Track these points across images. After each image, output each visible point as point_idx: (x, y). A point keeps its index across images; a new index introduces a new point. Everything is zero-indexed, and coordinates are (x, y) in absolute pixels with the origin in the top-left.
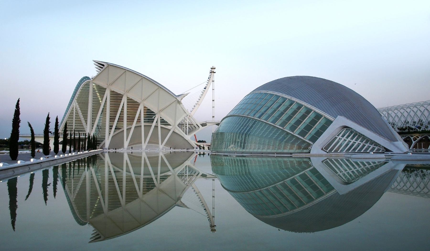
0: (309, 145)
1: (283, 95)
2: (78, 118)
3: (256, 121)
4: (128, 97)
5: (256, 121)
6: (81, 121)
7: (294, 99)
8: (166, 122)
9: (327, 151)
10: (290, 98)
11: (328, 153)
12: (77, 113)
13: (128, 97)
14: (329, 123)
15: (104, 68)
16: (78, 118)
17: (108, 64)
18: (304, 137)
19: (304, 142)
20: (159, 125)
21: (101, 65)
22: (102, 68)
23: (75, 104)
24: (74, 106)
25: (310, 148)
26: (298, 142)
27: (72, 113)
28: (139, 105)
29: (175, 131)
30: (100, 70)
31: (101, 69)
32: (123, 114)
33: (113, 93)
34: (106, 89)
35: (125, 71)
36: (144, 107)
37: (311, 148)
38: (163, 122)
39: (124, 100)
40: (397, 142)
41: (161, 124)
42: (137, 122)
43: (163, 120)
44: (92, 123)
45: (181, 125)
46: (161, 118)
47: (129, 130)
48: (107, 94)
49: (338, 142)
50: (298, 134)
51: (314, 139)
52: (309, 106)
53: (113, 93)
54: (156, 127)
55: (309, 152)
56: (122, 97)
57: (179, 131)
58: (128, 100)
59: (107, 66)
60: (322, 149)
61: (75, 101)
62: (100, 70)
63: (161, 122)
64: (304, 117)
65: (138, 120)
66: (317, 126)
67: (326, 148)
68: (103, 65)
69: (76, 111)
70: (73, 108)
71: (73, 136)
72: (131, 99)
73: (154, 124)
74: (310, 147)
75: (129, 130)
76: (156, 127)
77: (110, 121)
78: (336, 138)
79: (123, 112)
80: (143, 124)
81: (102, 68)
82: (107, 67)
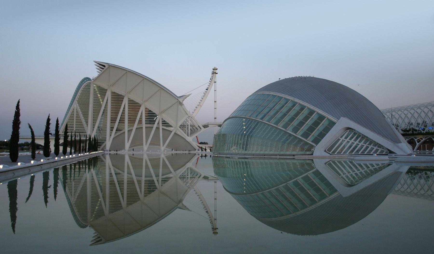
0: (312, 146)
1: (282, 95)
2: (78, 120)
3: (258, 123)
4: (129, 99)
5: (258, 122)
6: (81, 122)
7: (296, 100)
8: (168, 124)
9: (330, 153)
10: (293, 99)
11: (331, 154)
12: (77, 115)
13: (129, 99)
14: (332, 124)
15: (105, 68)
16: (78, 120)
17: (109, 65)
18: (306, 138)
19: (307, 143)
20: (161, 127)
21: (102, 66)
22: (103, 69)
23: (76, 105)
24: (74, 107)
25: (313, 150)
26: (301, 143)
27: (72, 114)
28: (140, 106)
29: (176, 133)
30: (101, 71)
31: (102, 70)
32: (124, 116)
33: (114, 94)
34: (107, 90)
35: (127, 72)
36: (145, 108)
37: (314, 150)
38: (165, 123)
39: (125, 102)
40: (401, 144)
41: (162, 126)
42: (138, 123)
43: (164, 121)
44: (93, 125)
45: (183, 127)
46: (162, 119)
47: (130, 131)
48: (109, 95)
49: (341, 144)
50: (301, 136)
51: (317, 141)
52: (312, 107)
53: (114, 94)
54: (158, 128)
55: (312, 154)
56: (123, 98)
57: (181, 132)
58: (129, 101)
59: (108, 67)
60: (325, 151)
61: (76, 102)
62: (101, 71)
63: (162, 123)
64: (306, 118)
65: (139, 121)
66: (320, 127)
67: (330, 150)
68: (104, 66)
69: (77, 112)
70: (74, 109)
71: (73, 138)
72: (132, 101)
73: (155, 125)
74: (313, 149)
75: (130, 131)
76: (158, 128)
77: (111, 123)
78: (339, 140)
79: (124, 113)
80: (144, 125)
81: (103, 69)
82: (108, 68)
